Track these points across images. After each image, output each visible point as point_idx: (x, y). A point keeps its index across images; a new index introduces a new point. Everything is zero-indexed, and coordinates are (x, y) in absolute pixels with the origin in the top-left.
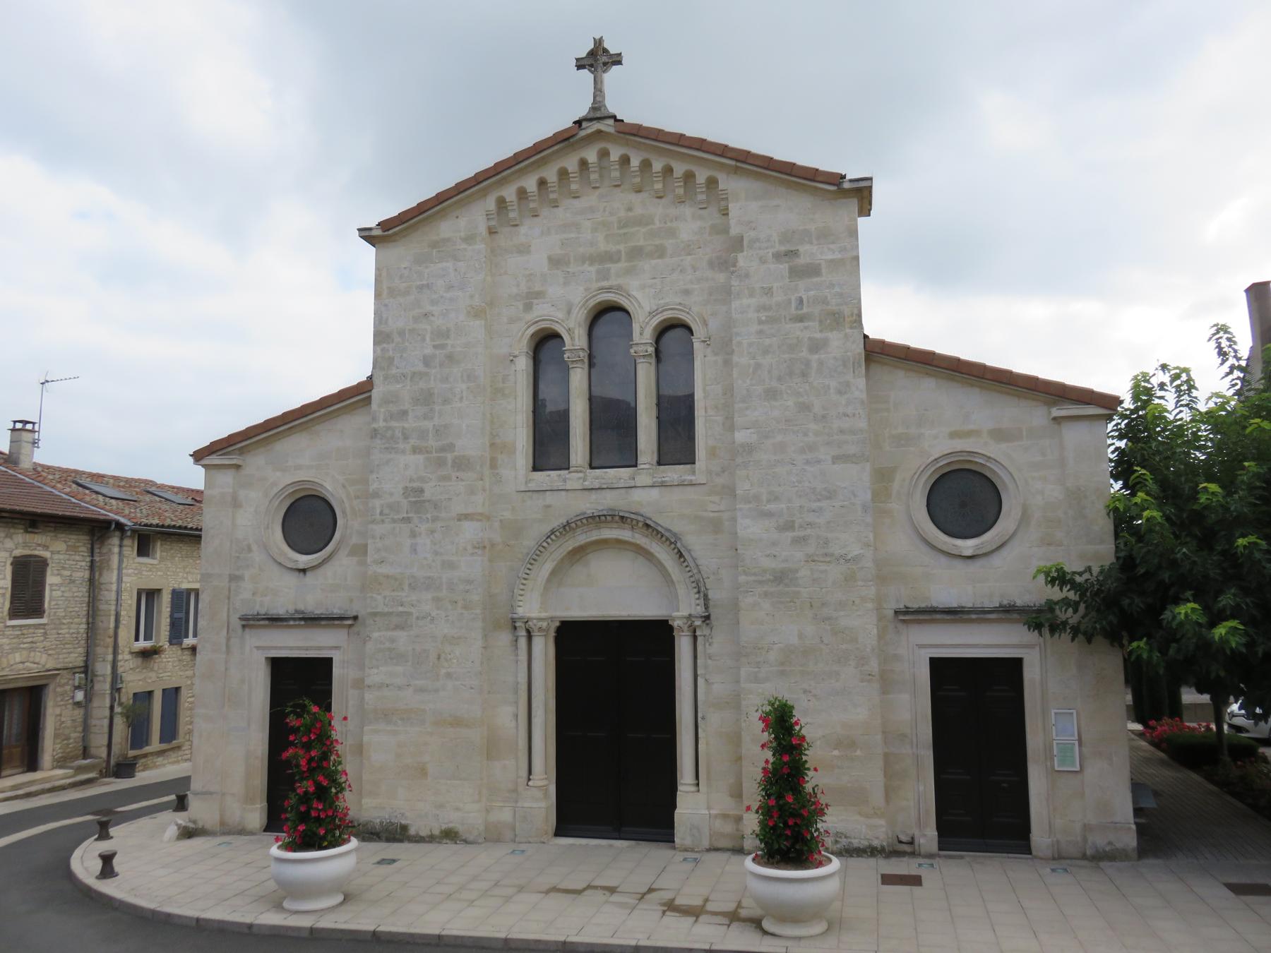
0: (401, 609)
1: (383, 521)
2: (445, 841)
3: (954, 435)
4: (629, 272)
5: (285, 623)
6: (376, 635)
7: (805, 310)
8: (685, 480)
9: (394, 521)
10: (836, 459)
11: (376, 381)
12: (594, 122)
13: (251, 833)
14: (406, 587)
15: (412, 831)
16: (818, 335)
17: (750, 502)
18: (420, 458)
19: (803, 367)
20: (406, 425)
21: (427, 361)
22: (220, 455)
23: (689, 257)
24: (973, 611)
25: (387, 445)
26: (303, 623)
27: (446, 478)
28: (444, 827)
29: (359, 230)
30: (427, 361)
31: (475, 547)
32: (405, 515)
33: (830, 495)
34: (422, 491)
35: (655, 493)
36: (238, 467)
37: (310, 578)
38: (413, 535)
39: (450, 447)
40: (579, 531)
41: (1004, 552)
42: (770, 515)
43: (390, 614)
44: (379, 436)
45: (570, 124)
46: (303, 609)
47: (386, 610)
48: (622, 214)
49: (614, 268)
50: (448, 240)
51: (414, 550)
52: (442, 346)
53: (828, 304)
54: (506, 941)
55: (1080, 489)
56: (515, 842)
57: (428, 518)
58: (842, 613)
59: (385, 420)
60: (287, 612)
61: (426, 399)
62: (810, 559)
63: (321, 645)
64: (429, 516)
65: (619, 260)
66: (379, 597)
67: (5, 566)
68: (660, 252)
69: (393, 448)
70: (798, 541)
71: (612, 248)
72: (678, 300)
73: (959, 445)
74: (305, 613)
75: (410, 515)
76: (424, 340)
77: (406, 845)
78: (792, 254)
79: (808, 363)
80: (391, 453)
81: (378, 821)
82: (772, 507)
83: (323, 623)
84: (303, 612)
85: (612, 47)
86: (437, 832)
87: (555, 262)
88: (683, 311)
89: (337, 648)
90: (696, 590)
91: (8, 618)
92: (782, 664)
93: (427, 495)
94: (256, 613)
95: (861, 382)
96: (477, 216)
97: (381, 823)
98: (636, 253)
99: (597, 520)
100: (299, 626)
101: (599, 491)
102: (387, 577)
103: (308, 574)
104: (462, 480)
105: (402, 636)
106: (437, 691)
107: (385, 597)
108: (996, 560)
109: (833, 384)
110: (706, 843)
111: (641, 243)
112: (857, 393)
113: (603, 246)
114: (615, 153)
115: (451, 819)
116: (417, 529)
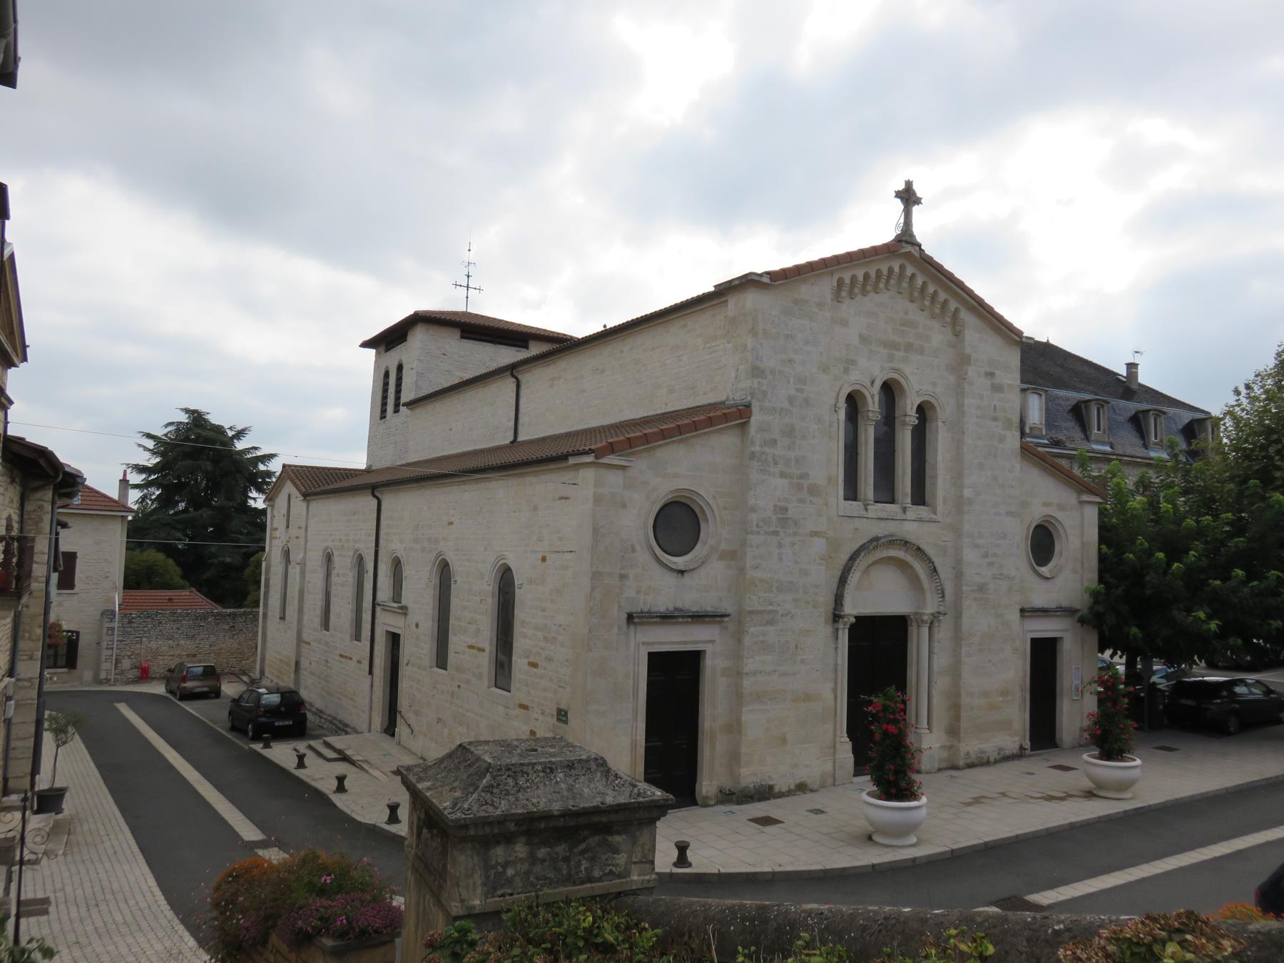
0: (771, 608)
1: (758, 533)
2: (798, 793)
5: (674, 621)
6: (752, 630)
8: (931, 518)
9: (767, 533)
12: (909, 245)
14: (774, 590)
15: (777, 789)
16: (1002, 432)
18: (785, 482)
20: (776, 453)
21: (791, 400)
22: (619, 456)
25: (762, 468)
26: (690, 620)
27: (802, 501)
28: (798, 782)
30: (791, 400)
31: (821, 559)
32: (774, 529)
34: (786, 510)
35: (915, 524)
36: (624, 468)
37: (687, 579)
38: (780, 546)
39: (804, 476)
43: (762, 612)
44: (756, 459)
46: (681, 607)
47: (760, 608)
51: (781, 560)
52: (801, 391)
54: (952, 851)
56: (835, 785)
57: (790, 533)
59: (761, 446)
60: (667, 609)
61: (790, 432)
62: (995, 578)
63: (697, 640)
64: (791, 531)
66: (754, 597)
68: (921, 351)
70: (991, 564)
74: (682, 611)
75: (777, 529)
76: (789, 382)
77: (772, 801)
78: (992, 375)
80: (764, 474)
81: (752, 785)
83: (707, 619)
84: (681, 610)
85: (901, 187)
86: (792, 787)
87: (864, 339)
88: (934, 397)
89: (712, 642)
90: (941, 595)
93: (790, 514)
94: (639, 610)
96: (823, 288)
97: (754, 787)
98: (909, 347)
100: (687, 623)
101: (886, 521)
102: (762, 581)
103: (686, 575)
104: (814, 504)
105: (770, 629)
106: (795, 674)
107: (759, 598)
110: (936, 766)
114: (909, 271)
115: (803, 775)
116: (782, 541)
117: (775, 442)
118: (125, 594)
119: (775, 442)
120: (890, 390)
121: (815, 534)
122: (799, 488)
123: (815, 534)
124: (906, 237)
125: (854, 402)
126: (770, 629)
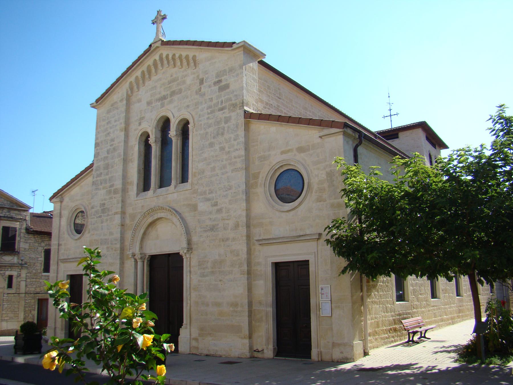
3: (283, 153)
10: (233, 171)
11: (95, 163)
16: (228, 115)
17: (202, 195)
19: (222, 131)
23: (189, 91)
27: (111, 198)
29: (90, 105)
42: (208, 200)
45: (148, 47)
55: (332, 172)
58: (234, 243)
67: (41, 253)
68: (180, 92)
69: (98, 188)
73: (285, 157)
78: (220, 81)
79: (224, 129)
82: (210, 196)
91: (43, 272)
98: (173, 93)
109: (232, 136)
113: (163, 93)
121: (116, 213)
123: (116, 213)
125: (145, 138)
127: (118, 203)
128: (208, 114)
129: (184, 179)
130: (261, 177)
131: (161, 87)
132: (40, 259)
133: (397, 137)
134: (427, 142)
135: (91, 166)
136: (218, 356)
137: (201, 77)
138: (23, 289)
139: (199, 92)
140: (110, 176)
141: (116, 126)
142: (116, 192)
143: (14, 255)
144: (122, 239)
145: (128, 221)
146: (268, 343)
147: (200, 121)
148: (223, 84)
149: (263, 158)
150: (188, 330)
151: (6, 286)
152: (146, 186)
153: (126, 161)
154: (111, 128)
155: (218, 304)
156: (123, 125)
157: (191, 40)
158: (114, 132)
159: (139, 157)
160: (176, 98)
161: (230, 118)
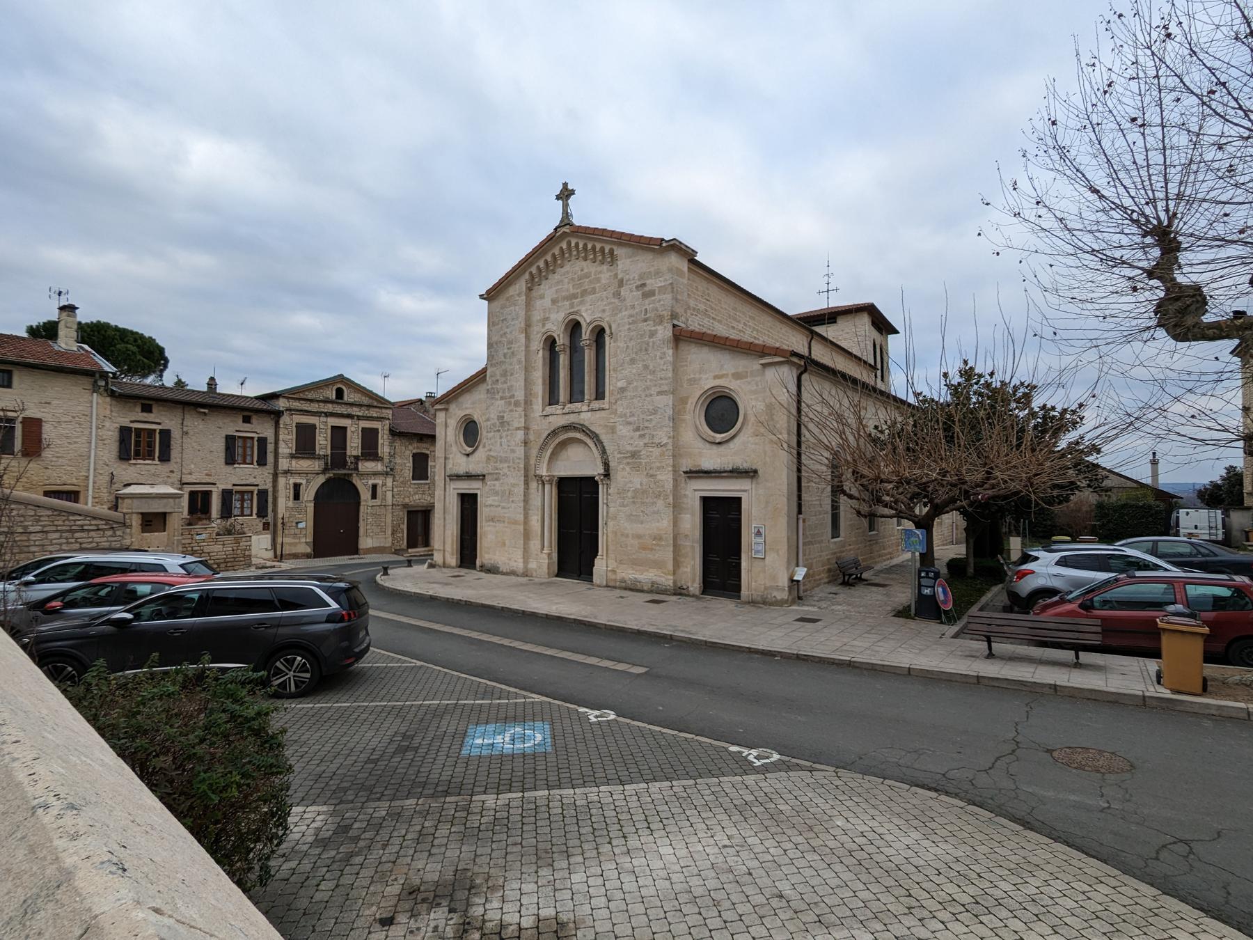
4: (582, 303)
7: (648, 315)
10: (659, 393)
11: (489, 367)
13: (453, 568)
15: (501, 570)
16: (653, 329)
24: (715, 472)
27: (511, 411)
30: (505, 355)
33: (655, 412)
34: (503, 417)
37: (471, 458)
38: (501, 438)
39: (513, 396)
40: (560, 434)
41: (736, 440)
42: (630, 423)
45: (552, 231)
48: (579, 273)
49: (576, 301)
50: (512, 296)
51: (501, 445)
53: (657, 311)
65: (577, 298)
68: (593, 291)
70: (642, 436)
71: (575, 291)
72: (600, 315)
78: (644, 285)
82: (631, 419)
87: (554, 301)
89: (478, 489)
92: (633, 498)
95: (670, 352)
96: (520, 285)
98: (584, 293)
99: (566, 428)
108: (731, 445)
111: (587, 287)
112: (668, 358)
113: (572, 291)
117: (497, 381)
118: (240, 459)
119: (497, 381)
120: (574, 327)
121: (518, 429)
122: (510, 403)
123: (518, 429)
124: (566, 220)
125: (551, 343)
126: (496, 482)
127: (521, 417)
128: (630, 324)
129: (600, 395)
130: (690, 402)
131: (569, 283)
132: (407, 465)
133: (835, 322)
134: (872, 328)
135: (484, 371)
136: (1207, 724)
137: (620, 276)
138: (389, 500)
139: (617, 295)
140: (509, 384)
141: (514, 325)
142: (517, 404)
143: (378, 460)
144: (527, 457)
145: (532, 437)
146: (694, 581)
147: (620, 331)
148: (647, 289)
149: (692, 382)
150: (604, 562)
151: (370, 497)
152: (553, 399)
153: (528, 369)
154: (507, 327)
155: (639, 537)
156: (523, 325)
157: (609, 229)
158: (511, 332)
159: (544, 365)
160: (589, 298)
161: (656, 331)
